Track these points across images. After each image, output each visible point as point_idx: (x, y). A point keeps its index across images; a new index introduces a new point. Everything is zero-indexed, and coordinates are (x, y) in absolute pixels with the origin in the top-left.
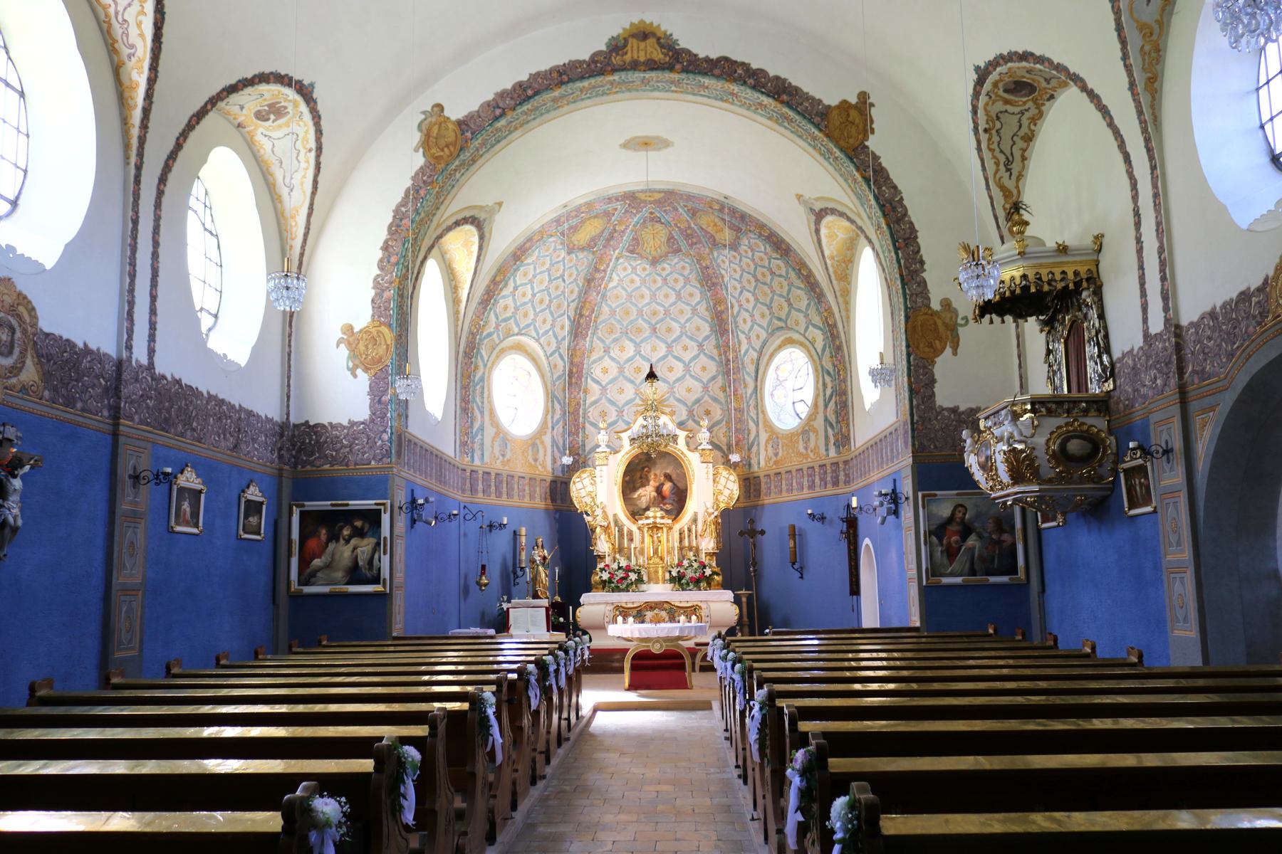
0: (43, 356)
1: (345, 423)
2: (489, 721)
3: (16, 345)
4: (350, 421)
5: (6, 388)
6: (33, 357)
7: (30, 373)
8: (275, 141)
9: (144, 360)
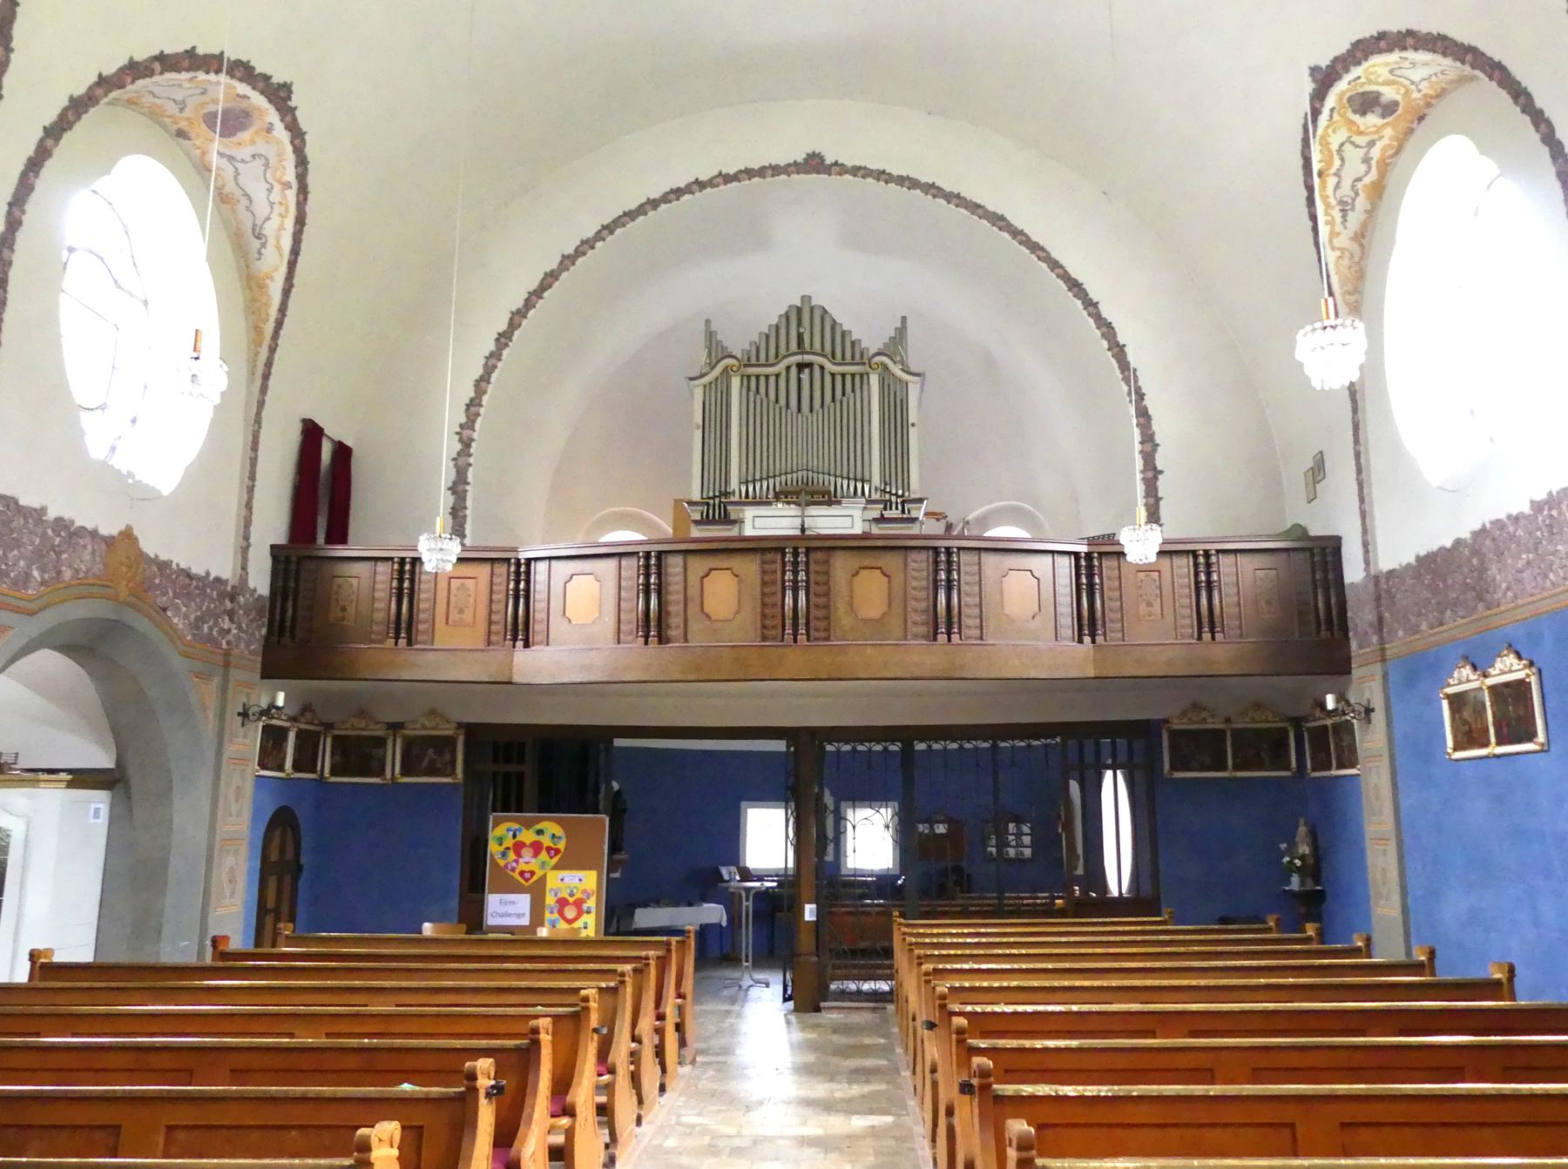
1: (1526, 509)
4: (128, 472)
8: (239, 165)
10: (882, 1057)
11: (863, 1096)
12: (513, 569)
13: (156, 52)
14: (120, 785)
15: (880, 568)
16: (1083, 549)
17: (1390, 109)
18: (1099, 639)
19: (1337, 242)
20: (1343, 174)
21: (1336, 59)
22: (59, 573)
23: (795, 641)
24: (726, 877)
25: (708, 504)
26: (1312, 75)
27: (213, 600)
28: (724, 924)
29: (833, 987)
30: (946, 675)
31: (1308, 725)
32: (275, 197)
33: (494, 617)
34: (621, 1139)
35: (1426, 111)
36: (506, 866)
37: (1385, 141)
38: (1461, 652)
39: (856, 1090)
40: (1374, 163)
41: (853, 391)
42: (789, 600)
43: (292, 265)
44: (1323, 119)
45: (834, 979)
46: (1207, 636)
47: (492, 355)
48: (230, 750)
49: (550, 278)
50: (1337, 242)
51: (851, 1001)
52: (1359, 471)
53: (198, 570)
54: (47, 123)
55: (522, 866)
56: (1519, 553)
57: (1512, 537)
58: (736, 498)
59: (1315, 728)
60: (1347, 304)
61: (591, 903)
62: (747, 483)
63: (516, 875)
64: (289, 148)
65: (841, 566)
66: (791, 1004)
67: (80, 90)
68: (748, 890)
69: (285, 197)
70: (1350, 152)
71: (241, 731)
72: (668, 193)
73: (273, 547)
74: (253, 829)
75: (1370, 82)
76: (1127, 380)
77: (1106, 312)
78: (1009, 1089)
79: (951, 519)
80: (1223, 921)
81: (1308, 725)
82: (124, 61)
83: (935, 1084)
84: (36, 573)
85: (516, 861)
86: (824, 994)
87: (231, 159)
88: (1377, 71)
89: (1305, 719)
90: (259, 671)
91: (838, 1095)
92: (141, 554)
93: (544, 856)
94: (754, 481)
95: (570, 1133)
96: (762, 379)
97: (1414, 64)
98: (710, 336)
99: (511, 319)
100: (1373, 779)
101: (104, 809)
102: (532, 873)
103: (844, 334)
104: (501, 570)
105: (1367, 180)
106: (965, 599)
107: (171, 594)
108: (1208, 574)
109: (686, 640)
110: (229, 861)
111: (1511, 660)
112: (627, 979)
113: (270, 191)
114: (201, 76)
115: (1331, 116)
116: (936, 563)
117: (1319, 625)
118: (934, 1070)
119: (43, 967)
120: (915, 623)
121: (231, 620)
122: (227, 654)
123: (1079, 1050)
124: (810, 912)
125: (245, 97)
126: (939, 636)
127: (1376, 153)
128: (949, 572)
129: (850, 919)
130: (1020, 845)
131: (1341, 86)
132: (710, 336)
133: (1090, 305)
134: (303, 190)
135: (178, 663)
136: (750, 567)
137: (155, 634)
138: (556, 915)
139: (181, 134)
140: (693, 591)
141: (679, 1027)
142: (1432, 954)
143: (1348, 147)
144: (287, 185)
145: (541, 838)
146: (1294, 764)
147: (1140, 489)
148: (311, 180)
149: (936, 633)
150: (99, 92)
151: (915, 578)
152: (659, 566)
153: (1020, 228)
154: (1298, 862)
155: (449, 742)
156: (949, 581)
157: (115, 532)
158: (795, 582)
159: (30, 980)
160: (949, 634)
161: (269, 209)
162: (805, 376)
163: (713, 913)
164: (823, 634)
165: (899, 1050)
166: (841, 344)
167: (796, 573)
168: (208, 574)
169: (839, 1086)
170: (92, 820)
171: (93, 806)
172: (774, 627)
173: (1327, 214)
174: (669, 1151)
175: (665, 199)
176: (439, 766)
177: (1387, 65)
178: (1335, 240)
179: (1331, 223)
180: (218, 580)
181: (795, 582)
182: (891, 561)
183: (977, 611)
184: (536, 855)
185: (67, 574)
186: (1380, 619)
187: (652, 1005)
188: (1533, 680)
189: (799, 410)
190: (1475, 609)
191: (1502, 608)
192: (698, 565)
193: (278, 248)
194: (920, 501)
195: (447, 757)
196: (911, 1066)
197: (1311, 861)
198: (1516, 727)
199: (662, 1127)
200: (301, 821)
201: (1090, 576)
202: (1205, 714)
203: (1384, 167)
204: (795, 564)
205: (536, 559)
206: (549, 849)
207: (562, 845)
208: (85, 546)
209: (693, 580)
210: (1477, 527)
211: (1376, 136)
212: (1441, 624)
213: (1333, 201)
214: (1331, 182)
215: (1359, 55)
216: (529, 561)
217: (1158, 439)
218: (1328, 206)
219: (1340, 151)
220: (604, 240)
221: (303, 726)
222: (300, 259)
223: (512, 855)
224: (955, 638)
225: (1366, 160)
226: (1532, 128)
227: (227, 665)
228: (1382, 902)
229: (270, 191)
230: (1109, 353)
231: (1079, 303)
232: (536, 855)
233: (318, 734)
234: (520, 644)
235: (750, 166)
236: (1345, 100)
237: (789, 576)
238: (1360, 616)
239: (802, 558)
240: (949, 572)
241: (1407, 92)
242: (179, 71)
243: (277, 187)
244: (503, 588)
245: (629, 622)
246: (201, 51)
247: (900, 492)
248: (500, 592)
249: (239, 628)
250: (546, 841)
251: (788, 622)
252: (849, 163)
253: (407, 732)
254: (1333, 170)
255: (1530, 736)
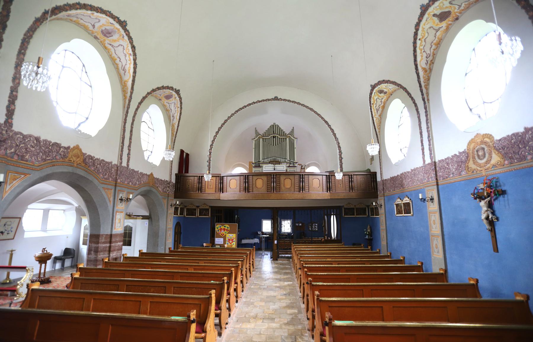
0: (500, 149)
1: (410, 170)
2: (55, 15)
3: (486, 153)
5: (486, 170)
6: (495, 152)
7: (496, 158)
9: (334, 210)
10: (290, 270)
11: (286, 278)
12: (220, 178)
13: (157, 87)
14: (150, 219)
15: (290, 178)
16: (328, 174)
17: (385, 93)
18: (331, 191)
19: (376, 116)
20: (377, 104)
21: (375, 84)
22: (141, 182)
23: (274, 192)
24: (259, 234)
25: (256, 163)
26: (371, 86)
27: (166, 185)
28: (259, 243)
29: (280, 256)
30: (302, 199)
31: (370, 207)
32: (176, 110)
33: (217, 187)
34: (244, 287)
35: (392, 93)
36: (219, 233)
37: (385, 98)
38: (398, 196)
39: (285, 277)
40: (383, 102)
41: (284, 141)
42: (272, 184)
43: (179, 122)
44: (373, 94)
45: (280, 254)
46: (351, 191)
47: (215, 136)
48: (169, 212)
49: (226, 121)
50: (376, 116)
51: (283, 258)
52: (380, 160)
53: (163, 179)
54: (139, 102)
55: (222, 233)
56: (409, 179)
57: (408, 175)
58: (261, 162)
59: (371, 208)
60: (378, 128)
61: (235, 240)
62: (263, 159)
63: (221, 235)
64: (179, 101)
65: (282, 178)
66: (272, 259)
67: (144, 95)
68: (264, 237)
69: (178, 109)
70: (379, 101)
71: (171, 208)
72: (248, 105)
73: (176, 174)
74: (173, 226)
75: (382, 88)
76: (336, 140)
77: (332, 127)
78: (315, 283)
79: (302, 165)
80: (354, 244)
81: (370, 207)
82: (152, 89)
83: (301, 278)
84: (137, 183)
85: (221, 232)
86: (278, 257)
87: (169, 103)
88: (383, 86)
89: (370, 206)
90: (173, 196)
91: (282, 278)
92: (154, 177)
93: (226, 231)
94: (265, 159)
95: (237, 287)
96: (266, 139)
97: (390, 86)
98: (256, 131)
99: (219, 129)
100: (382, 218)
101: (147, 223)
102: (224, 234)
103: (282, 130)
104: (218, 178)
105: (381, 105)
106: (306, 184)
107: (159, 184)
108: (352, 179)
109: (253, 192)
110: (169, 232)
111: (407, 198)
112: (245, 259)
113: (175, 109)
114: (164, 90)
115: (375, 94)
116: (300, 177)
117: (372, 189)
118: (300, 276)
119: (141, 253)
120: (296, 189)
121: (169, 188)
122: (168, 195)
123: (327, 275)
124: (276, 242)
125: (172, 93)
126: (301, 191)
127: (383, 100)
128: (303, 179)
129: (283, 243)
130: (315, 228)
131: (376, 89)
132: (256, 131)
133: (329, 126)
134: (181, 108)
135: (160, 197)
136: (265, 178)
137: (156, 192)
138: (228, 242)
139: (160, 100)
140: (254, 183)
141: (253, 265)
142: (391, 254)
143: (378, 99)
144: (179, 107)
145: (225, 228)
146: (367, 214)
147: (339, 161)
148: (183, 106)
149: (300, 191)
150: (148, 95)
151: (296, 179)
152: (248, 178)
153: (316, 111)
154: (368, 233)
155: (208, 210)
156: (303, 181)
157: (150, 174)
158: (274, 181)
159: (139, 256)
160: (303, 191)
161: (175, 112)
162: (274, 139)
163: (256, 241)
164: (279, 191)
165: (293, 269)
166: (282, 133)
167: (274, 179)
168: (165, 180)
169: (282, 276)
170: (146, 225)
171: (146, 222)
172: (269, 190)
173: (374, 111)
174: (252, 288)
175: (248, 105)
176: (206, 214)
177: (385, 85)
178: (375, 116)
179: (375, 113)
180: (166, 181)
181: (274, 181)
182: (292, 177)
183: (308, 186)
184: (224, 231)
185: (142, 182)
186: (384, 188)
187: (249, 262)
188: (411, 203)
189: (273, 145)
190: (401, 188)
191: (405, 189)
192: (255, 178)
193: (177, 119)
194: (297, 163)
195: (208, 212)
196: (295, 272)
197: (370, 233)
198: (408, 211)
199: (250, 284)
200: (181, 224)
201: (329, 179)
202: (351, 205)
203: (385, 103)
204: (274, 177)
205: (224, 176)
206: (227, 230)
207: (229, 229)
208: (145, 177)
209: (254, 180)
210: (401, 173)
211: (383, 98)
212: (395, 190)
213: (375, 109)
214: (375, 105)
215: (380, 83)
216: (223, 176)
217: (342, 152)
218: (374, 110)
219: (376, 100)
220: (236, 113)
221: (181, 207)
222: (180, 120)
223: (220, 231)
224: (304, 191)
225: (381, 102)
226: (411, 100)
227: (168, 196)
228: (383, 241)
229: (175, 109)
230: (333, 135)
231: (327, 125)
232: (224, 231)
233: (184, 208)
234: (221, 192)
235: (264, 99)
236: (377, 91)
237: (272, 180)
238: (380, 187)
239: (275, 176)
240: (303, 179)
241: (389, 90)
242: (160, 90)
243: (177, 108)
244: (218, 181)
245: (242, 188)
246: (164, 86)
247: (293, 161)
248: (217, 182)
249: (170, 190)
250: (226, 228)
251: (272, 189)
252: (283, 98)
253: (200, 208)
254: (375, 103)
255: (410, 213)
